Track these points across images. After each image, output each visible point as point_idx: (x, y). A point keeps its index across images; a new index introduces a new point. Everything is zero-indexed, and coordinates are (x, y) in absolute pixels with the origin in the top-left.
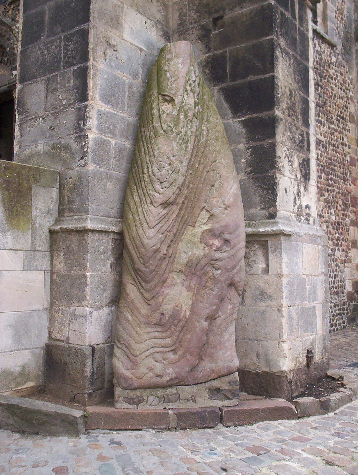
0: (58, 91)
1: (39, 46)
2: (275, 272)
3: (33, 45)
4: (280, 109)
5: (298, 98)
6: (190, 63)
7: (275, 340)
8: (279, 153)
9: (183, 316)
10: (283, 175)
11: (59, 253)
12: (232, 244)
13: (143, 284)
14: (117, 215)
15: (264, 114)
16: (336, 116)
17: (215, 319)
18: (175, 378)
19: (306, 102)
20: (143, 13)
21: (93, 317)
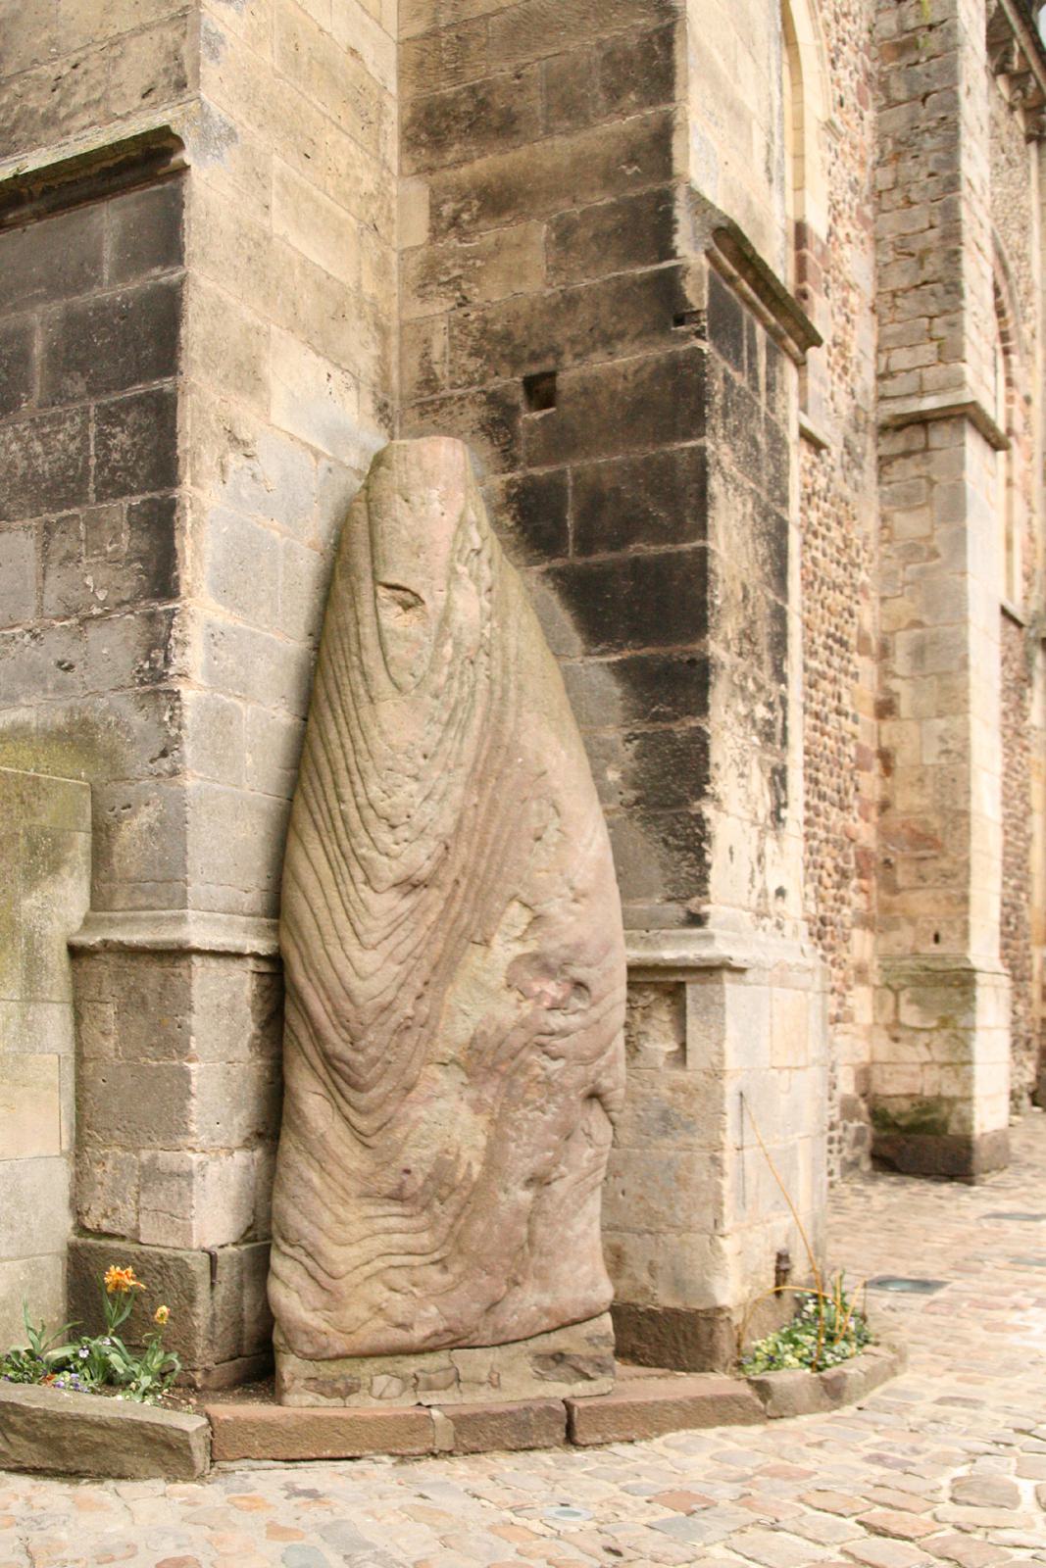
1: (15, 430)
2: (706, 1065)
6: (466, 499)
7: (703, 1231)
8: (716, 755)
10: (726, 812)
12: (595, 992)
14: (258, 908)
15: (678, 651)
16: (823, 638)
17: (549, 1184)
18: (448, 1330)
19: (780, 615)
21: (208, 1177)
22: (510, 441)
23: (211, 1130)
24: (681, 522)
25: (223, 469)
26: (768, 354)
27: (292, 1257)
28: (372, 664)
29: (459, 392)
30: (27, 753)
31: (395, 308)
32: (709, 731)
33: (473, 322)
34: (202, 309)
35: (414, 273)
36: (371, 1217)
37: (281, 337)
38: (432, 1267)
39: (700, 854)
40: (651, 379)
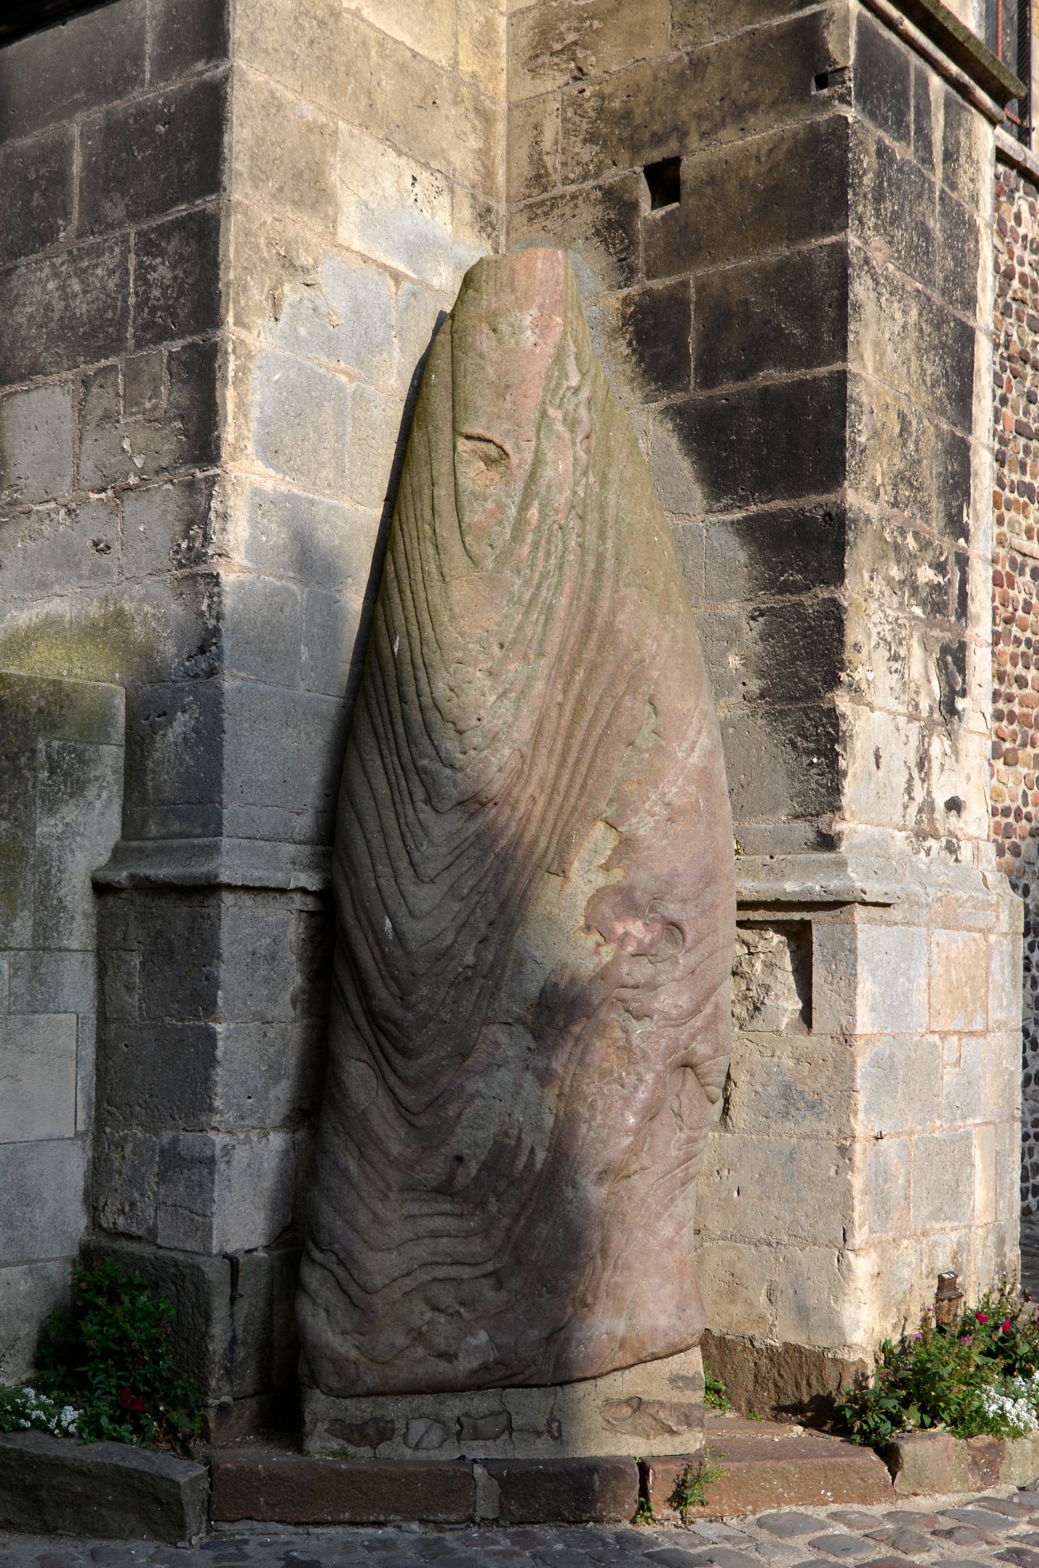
0: (118, 421)
1: (53, 264)
3: (34, 257)
4: (864, 484)
5: (931, 443)
8: (853, 633)
9: (525, 1167)
11: (125, 956)
13: (397, 1060)
15: (812, 502)
18: (498, 1362)
20: (405, 150)
21: (234, 1164)
22: (627, 248)
23: (239, 1106)
24: (817, 339)
25: (276, 304)
26: (947, 114)
27: (322, 1266)
28: (445, 534)
29: (572, 188)
30: (59, 652)
31: (503, 86)
32: (846, 604)
33: (588, 100)
34: (251, 109)
35: (525, 41)
36: (414, 1216)
37: (351, 135)
38: (483, 1281)
39: (833, 758)
40: (786, 159)
